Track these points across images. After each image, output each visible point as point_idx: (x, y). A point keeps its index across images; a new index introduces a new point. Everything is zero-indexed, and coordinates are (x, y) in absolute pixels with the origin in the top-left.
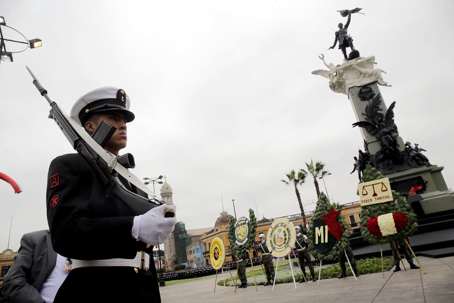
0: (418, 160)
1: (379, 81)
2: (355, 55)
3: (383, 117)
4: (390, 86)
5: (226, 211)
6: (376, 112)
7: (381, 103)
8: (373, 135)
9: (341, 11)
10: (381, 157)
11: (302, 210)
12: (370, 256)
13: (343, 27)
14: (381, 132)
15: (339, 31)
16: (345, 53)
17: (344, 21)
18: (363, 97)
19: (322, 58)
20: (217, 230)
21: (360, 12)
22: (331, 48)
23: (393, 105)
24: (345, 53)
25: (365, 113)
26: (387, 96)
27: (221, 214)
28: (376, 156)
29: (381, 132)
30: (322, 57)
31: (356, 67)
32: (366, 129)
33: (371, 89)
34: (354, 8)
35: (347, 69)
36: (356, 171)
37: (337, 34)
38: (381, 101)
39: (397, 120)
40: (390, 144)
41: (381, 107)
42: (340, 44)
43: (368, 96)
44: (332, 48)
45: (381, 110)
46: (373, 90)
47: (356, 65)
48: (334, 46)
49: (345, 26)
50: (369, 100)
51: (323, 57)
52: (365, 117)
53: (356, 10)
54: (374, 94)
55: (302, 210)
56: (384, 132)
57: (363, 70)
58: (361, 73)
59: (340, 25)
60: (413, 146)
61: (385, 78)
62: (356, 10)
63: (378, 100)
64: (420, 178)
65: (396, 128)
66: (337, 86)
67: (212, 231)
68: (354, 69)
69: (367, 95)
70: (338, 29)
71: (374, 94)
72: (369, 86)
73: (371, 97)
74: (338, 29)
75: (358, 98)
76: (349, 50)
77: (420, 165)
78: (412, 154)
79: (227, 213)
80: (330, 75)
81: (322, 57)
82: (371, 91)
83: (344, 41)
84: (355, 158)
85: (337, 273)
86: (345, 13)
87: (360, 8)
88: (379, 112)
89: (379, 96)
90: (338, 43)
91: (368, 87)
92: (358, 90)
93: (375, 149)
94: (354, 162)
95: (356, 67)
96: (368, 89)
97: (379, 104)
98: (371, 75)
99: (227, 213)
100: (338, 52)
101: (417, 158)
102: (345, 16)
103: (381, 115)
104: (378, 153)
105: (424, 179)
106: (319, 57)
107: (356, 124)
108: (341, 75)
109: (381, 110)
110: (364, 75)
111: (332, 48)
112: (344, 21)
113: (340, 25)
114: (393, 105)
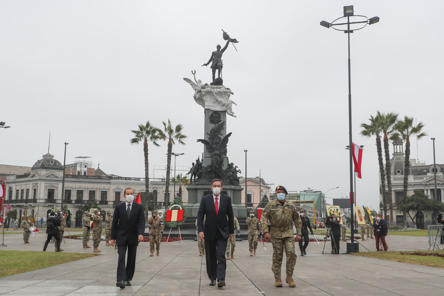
2: (218, 82)
3: (220, 140)
4: (236, 117)
5: (51, 153)
6: (217, 135)
8: (210, 152)
10: (209, 170)
13: (220, 50)
14: (214, 153)
17: (223, 43)
18: (212, 120)
19: (194, 73)
20: (33, 176)
23: (230, 134)
25: (209, 133)
26: (231, 124)
27: (44, 156)
28: (206, 168)
29: (214, 153)
32: (206, 146)
33: (220, 116)
36: (190, 174)
37: (214, 54)
38: (223, 128)
40: (217, 163)
41: (222, 132)
44: (206, 65)
45: (222, 135)
46: (222, 116)
50: (215, 124)
52: (209, 136)
53: (234, 41)
54: (221, 121)
56: (216, 153)
57: (219, 99)
58: (217, 100)
59: (219, 47)
62: (234, 41)
63: (222, 126)
65: (226, 152)
66: (199, 99)
67: (26, 176)
68: (213, 95)
69: (216, 120)
70: (215, 50)
74: (215, 50)
77: (232, 184)
78: (228, 174)
79: (53, 156)
82: (219, 117)
83: (216, 62)
84: (193, 164)
86: (226, 37)
88: (219, 136)
89: (224, 124)
90: (211, 63)
92: (211, 113)
94: (191, 166)
97: (221, 130)
98: (223, 105)
99: (53, 156)
100: (209, 69)
101: (231, 178)
103: (220, 138)
104: (208, 166)
106: (192, 71)
107: (199, 140)
109: (222, 135)
110: (219, 103)
111: (206, 65)
112: (223, 43)
113: (219, 47)
114: (230, 134)
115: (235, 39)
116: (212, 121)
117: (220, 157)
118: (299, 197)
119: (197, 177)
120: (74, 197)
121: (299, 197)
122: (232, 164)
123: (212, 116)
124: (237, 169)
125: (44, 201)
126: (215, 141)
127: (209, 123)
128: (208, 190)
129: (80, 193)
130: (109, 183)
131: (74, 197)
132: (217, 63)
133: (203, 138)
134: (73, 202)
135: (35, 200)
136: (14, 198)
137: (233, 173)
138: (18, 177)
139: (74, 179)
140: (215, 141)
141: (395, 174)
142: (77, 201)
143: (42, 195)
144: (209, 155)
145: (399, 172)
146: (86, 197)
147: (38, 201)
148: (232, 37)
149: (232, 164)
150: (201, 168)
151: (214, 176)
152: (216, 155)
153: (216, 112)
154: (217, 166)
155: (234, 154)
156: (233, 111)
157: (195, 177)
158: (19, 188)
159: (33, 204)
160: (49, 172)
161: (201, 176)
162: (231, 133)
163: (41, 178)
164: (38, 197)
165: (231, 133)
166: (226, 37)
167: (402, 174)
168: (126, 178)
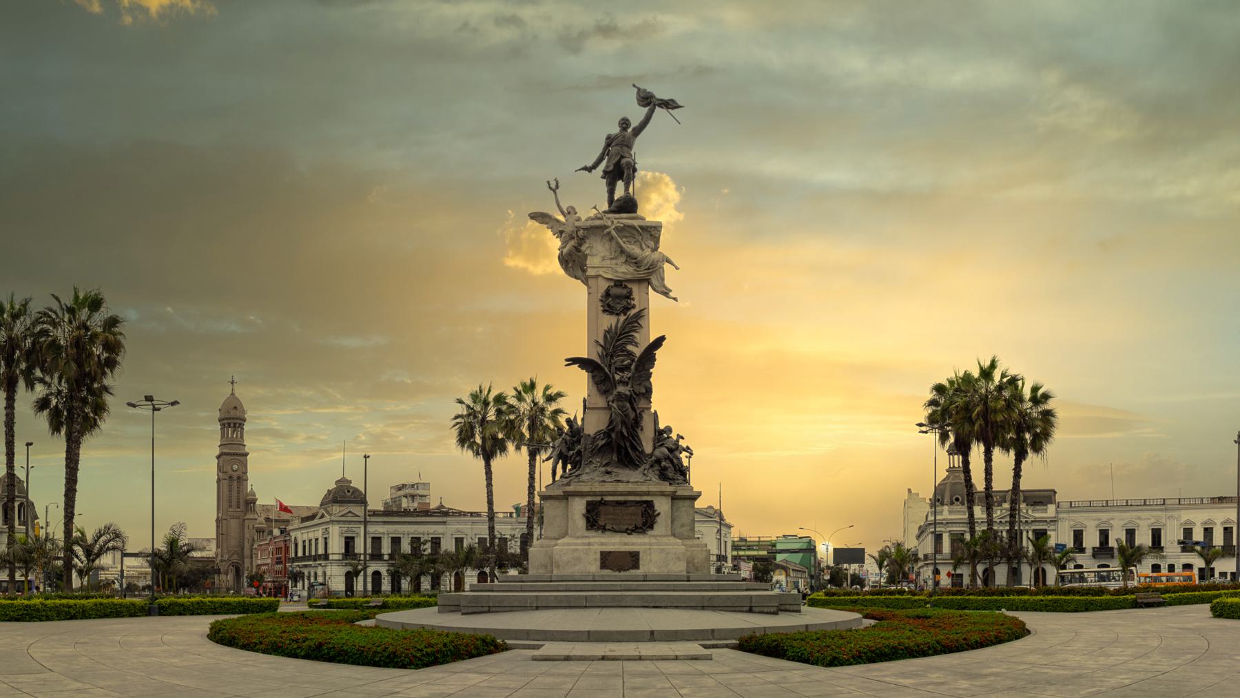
0: (665, 469)
1: (654, 281)
2: (628, 206)
4: (675, 299)
7: (642, 331)
8: (605, 393)
9: (639, 89)
10: (601, 443)
11: (490, 503)
12: (642, 675)
15: (616, 137)
16: (611, 192)
18: (609, 305)
20: (323, 516)
21: (674, 112)
22: (585, 168)
23: (659, 342)
24: (611, 192)
26: (658, 314)
30: (553, 186)
31: (614, 233)
33: (630, 293)
34: (666, 97)
35: (595, 230)
37: (610, 141)
39: (659, 375)
42: (607, 166)
43: (619, 307)
46: (635, 294)
47: (617, 229)
48: (595, 166)
49: (634, 129)
50: (618, 314)
51: (557, 187)
52: (600, 349)
53: (669, 105)
54: (634, 307)
55: (490, 503)
58: (622, 251)
59: (625, 124)
60: (674, 436)
61: (670, 276)
62: (669, 105)
63: (636, 321)
64: (650, 504)
65: (649, 391)
67: (313, 517)
70: (616, 130)
71: (634, 307)
72: (629, 286)
73: (626, 309)
74: (616, 130)
75: (600, 304)
76: (619, 192)
77: (671, 481)
80: (561, 232)
81: (553, 186)
82: (629, 296)
85: (110, 545)
86: (646, 99)
87: (680, 104)
88: (630, 348)
89: (640, 315)
91: (626, 287)
92: (604, 285)
93: (594, 425)
95: (614, 233)
96: (625, 292)
102: (645, 106)
103: (630, 354)
105: (656, 507)
107: (574, 361)
108: (582, 240)
109: (636, 345)
112: (637, 114)
114: (659, 342)
115: (673, 101)
116: (609, 309)
117: (631, 404)
118: (774, 545)
119: (569, 466)
120: (386, 549)
121: (774, 545)
122: (669, 430)
123: (607, 294)
124: (682, 443)
125: (340, 557)
126: (619, 360)
127: (600, 313)
128: (599, 499)
129: (396, 541)
130: (444, 523)
131: (386, 549)
132: (619, 161)
133: (584, 355)
134: (386, 557)
135: (326, 556)
136: (300, 554)
137: (671, 451)
138: (304, 520)
139: (385, 519)
140: (619, 360)
141: (952, 503)
142: (391, 556)
143: (336, 547)
144: (601, 402)
145: (957, 500)
146: (406, 547)
147: (331, 557)
148: (661, 93)
149: (669, 430)
150: (579, 441)
151: (615, 458)
152: (620, 397)
153: (619, 283)
154: (624, 431)
155: (671, 401)
156: (667, 283)
157: (564, 468)
158: (305, 537)
159: (323, 563)
160: (345, 509)
161: (580, 461)
162: (662, 339)
163: (333, 518)
164: (330, 551)
165: (662, 339)
166: (646, 99)
167: (963, 504)
168: (472, 514)
